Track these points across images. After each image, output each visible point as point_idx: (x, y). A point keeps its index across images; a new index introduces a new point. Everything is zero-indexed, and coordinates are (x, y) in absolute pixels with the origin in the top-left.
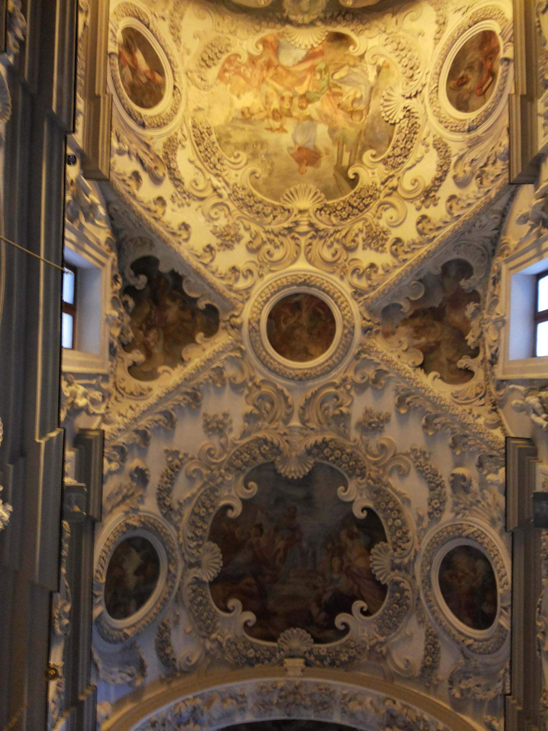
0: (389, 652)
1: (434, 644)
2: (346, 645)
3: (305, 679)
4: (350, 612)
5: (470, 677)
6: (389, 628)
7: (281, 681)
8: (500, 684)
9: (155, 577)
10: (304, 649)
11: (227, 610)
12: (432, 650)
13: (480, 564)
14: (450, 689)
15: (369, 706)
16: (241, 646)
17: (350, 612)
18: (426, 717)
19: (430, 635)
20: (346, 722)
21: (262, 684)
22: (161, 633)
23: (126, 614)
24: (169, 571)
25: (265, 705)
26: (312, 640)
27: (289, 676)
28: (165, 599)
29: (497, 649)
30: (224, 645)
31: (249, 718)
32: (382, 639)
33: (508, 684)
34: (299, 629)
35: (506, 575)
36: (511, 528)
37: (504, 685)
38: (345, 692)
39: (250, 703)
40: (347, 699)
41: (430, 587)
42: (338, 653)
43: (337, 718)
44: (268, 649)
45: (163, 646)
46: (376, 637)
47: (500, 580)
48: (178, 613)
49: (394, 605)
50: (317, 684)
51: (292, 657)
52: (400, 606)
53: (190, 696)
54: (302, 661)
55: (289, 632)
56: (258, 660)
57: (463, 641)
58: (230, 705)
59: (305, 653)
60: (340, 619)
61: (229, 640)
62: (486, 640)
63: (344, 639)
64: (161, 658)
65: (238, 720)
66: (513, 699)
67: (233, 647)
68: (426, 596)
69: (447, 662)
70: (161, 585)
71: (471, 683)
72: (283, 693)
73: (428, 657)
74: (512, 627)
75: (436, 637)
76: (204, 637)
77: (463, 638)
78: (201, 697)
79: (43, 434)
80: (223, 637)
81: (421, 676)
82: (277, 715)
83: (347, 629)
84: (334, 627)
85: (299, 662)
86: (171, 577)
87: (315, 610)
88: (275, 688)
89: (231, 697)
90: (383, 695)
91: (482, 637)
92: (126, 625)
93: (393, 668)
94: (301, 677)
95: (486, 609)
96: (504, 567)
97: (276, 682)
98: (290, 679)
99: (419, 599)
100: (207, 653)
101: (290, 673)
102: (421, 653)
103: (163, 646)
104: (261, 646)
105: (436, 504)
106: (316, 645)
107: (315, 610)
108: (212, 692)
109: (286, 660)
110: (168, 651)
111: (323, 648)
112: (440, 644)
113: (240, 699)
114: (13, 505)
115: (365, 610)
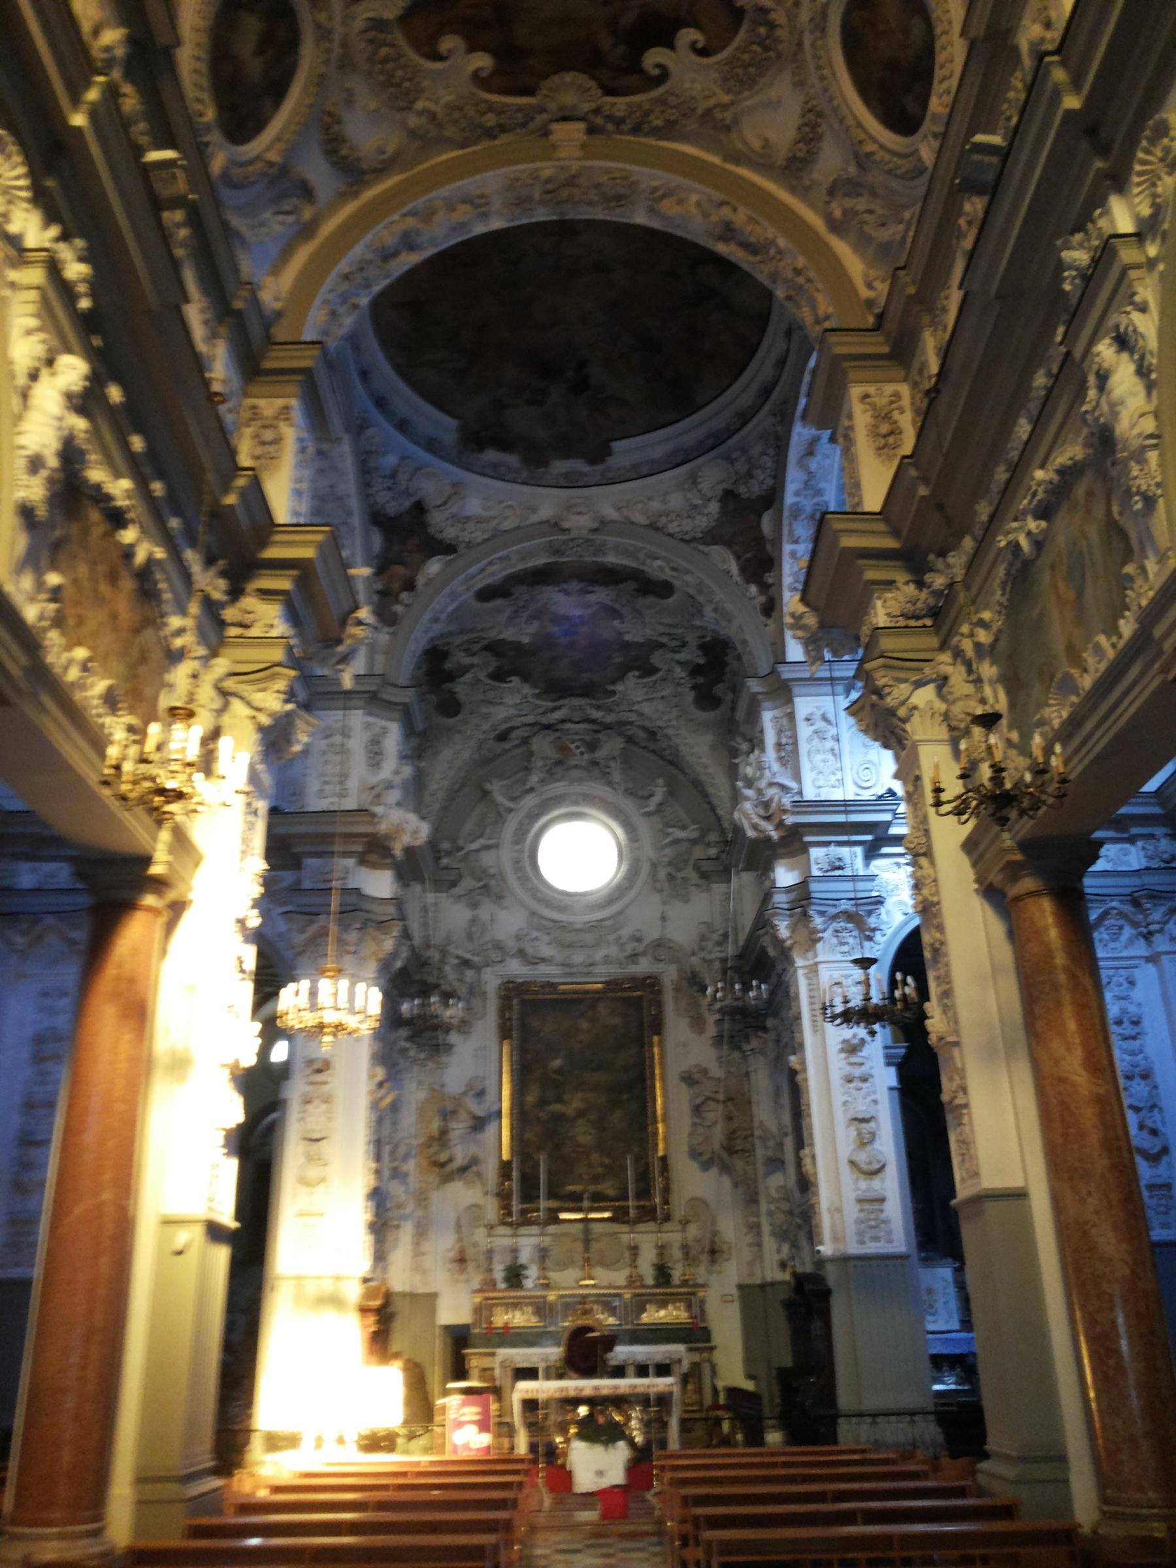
0: (736, 121)
1: (814, 126)
2: (662, 101)
3: (589, 163)
4: (671, 46)
5: (861, 195)
6: (740, 81)
7: (547, 169)
8: (901, 227)
9: (292, 44)
10: (586, 107)
11: (439, 58)
12: (810, 134)
13: (917, 24)
14: (828, 203)
15: (694, 210)
16: (470, 111)
17: (671, 46)
18: (782, 242)
19: (810, 111)
20: (656, 224)
21: (512, 176)
22: (327, 128)
23: (259, 125)
24: (319, 26)
25: (522, 203)
26: (599, 92)
27: (559, 159)
28: (322, 76)
29: (913, 179)
30: (439, 116)
31: (497, 224)
32: (726, 99)
33: (911, 234)
34: (576, 74)
35: (951, 76)
36: (972, 35)
37: (907, 230)
38: (654, 184)
39: (497, 204)
40: (657, 196)
41: (823, 30)
42: (646, 114)
43: (640, 218)
44: (520, 109)
45: (334, 146)
46: (715, 94)
47: (941, 82)
48: (348, 85)
49: (755, 47)
50: (608, 171)
51: (565, 119)
52: (767, 49)
53: (396, 217)
54: (581, 126)
55: (556, 79)
56: (503, 129)
57: (860, 142)
58: (463, 212)
59: (587, 113)
60: (654, 58)
61: (447, 105)
62: (901, 156)
63: (660, 91)
64: (334, 164)
65: (479, 229)
66: (907, 275)
67: (456, 115)
68: (813, 45)
69: (831, 161)
70: (309, 56)
71: (861, 204)
72: (550, 187)
73: (801, 145)
74: (936, 165)
75: (820, 115)
76: (402, 109)
77: (863, 136)
78: (411, 214)
79: (76, 100)
80: (437, 103)
81: (786, 168)
82: (542, 215)
83: (664, 75)
84: (640, 70)
85: (576, 129)
86: (323, 34)
87: (605, 42)
88: (537, 178)
89: (464, 202)
90: (718, 196)
91: (895, 147)
92: (264, 146)
93: (740, 146)
94: (580, 159)
95: (911, 106)
96: (952, 61)
97: (537, 170)
98: (562, 163)
99: (800, 45)
100: (412, 133)
101: (562, 153)
102: (791, 134)
103: (334, 146)
104: (508, 105)
105: (800, 150)
106: (610, 99)
107: (605, 42)
108: (429, 201)
109: (555, 126)
110: (344, 152)
111: (620, 105)
112: (823, 128)
113: (479, 204)
114: (83, 235)
115: (700, 45)
